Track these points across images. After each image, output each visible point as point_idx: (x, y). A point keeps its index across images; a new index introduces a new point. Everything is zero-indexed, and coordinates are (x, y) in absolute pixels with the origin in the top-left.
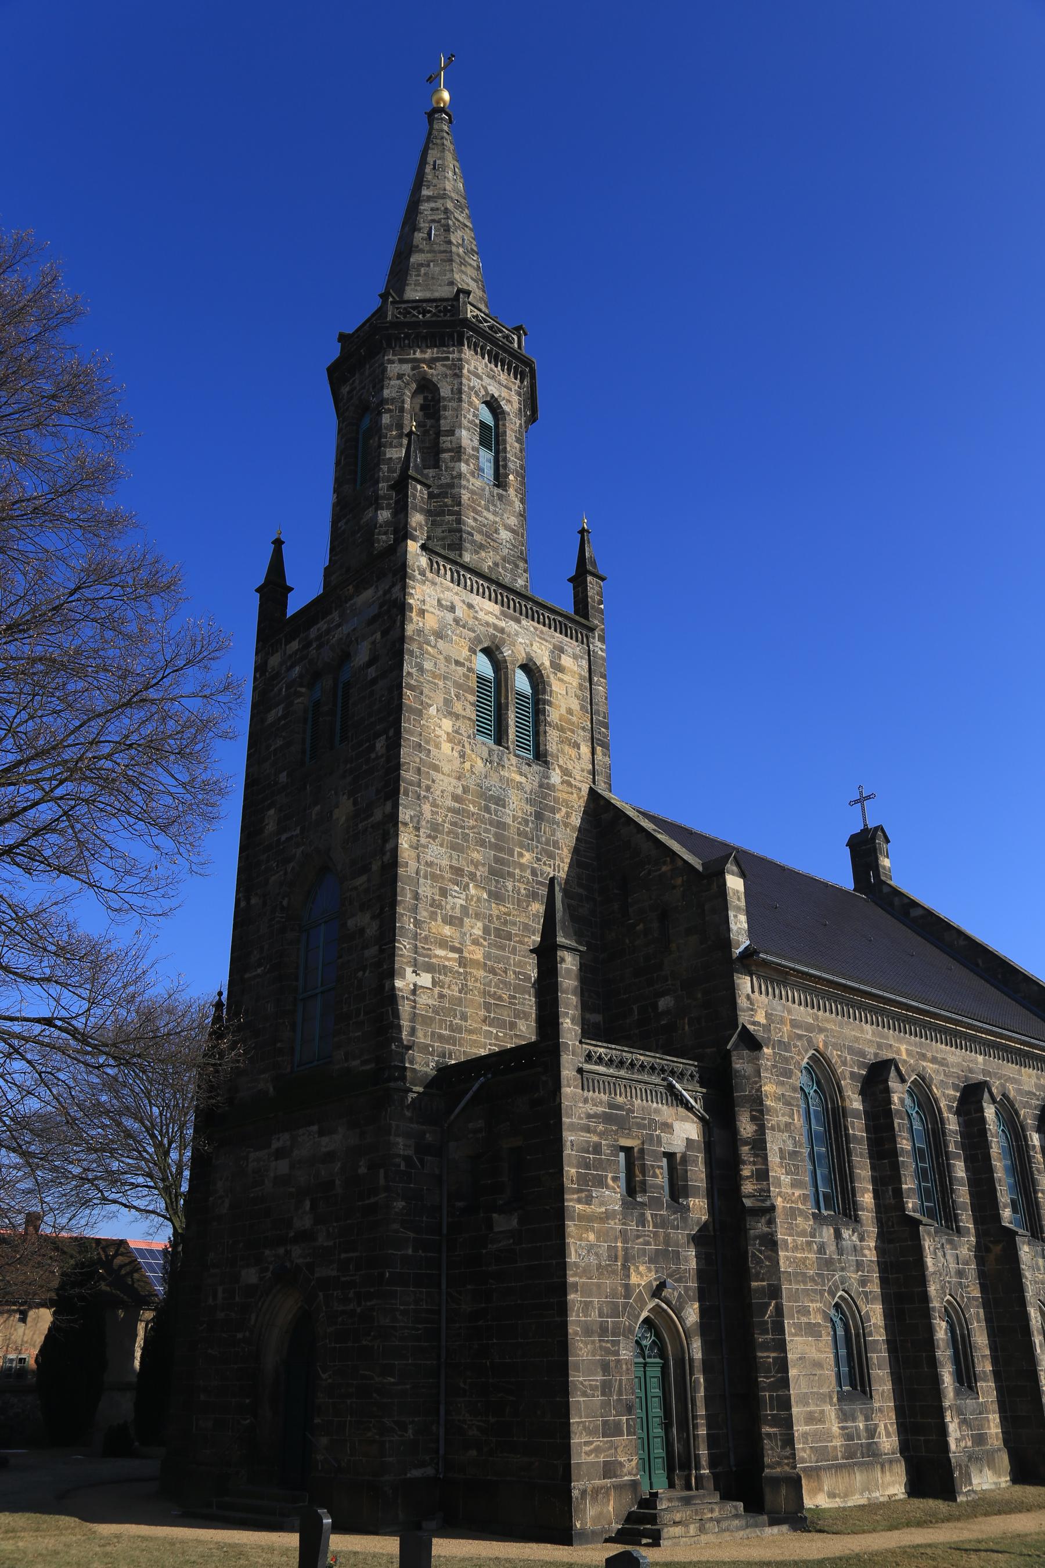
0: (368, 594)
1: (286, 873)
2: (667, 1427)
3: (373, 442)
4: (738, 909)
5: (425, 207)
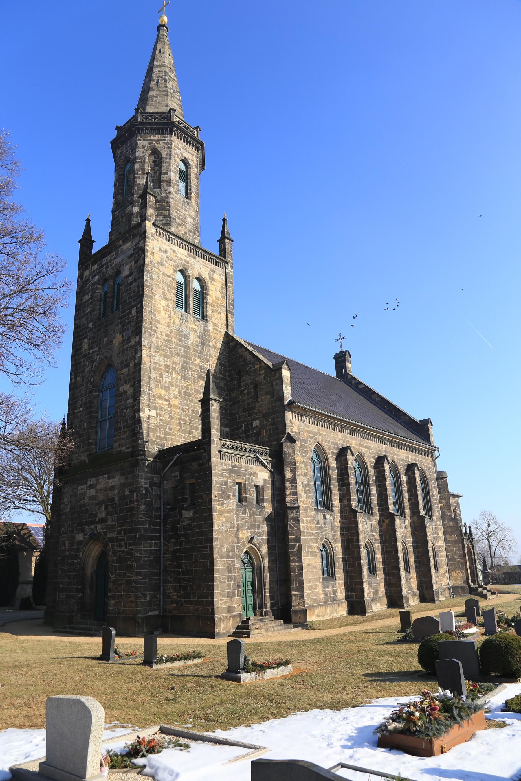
0: (128, 245)
1: (92, 367)
2: (254, 593)
3: (131, 177)
5: (155, 70)
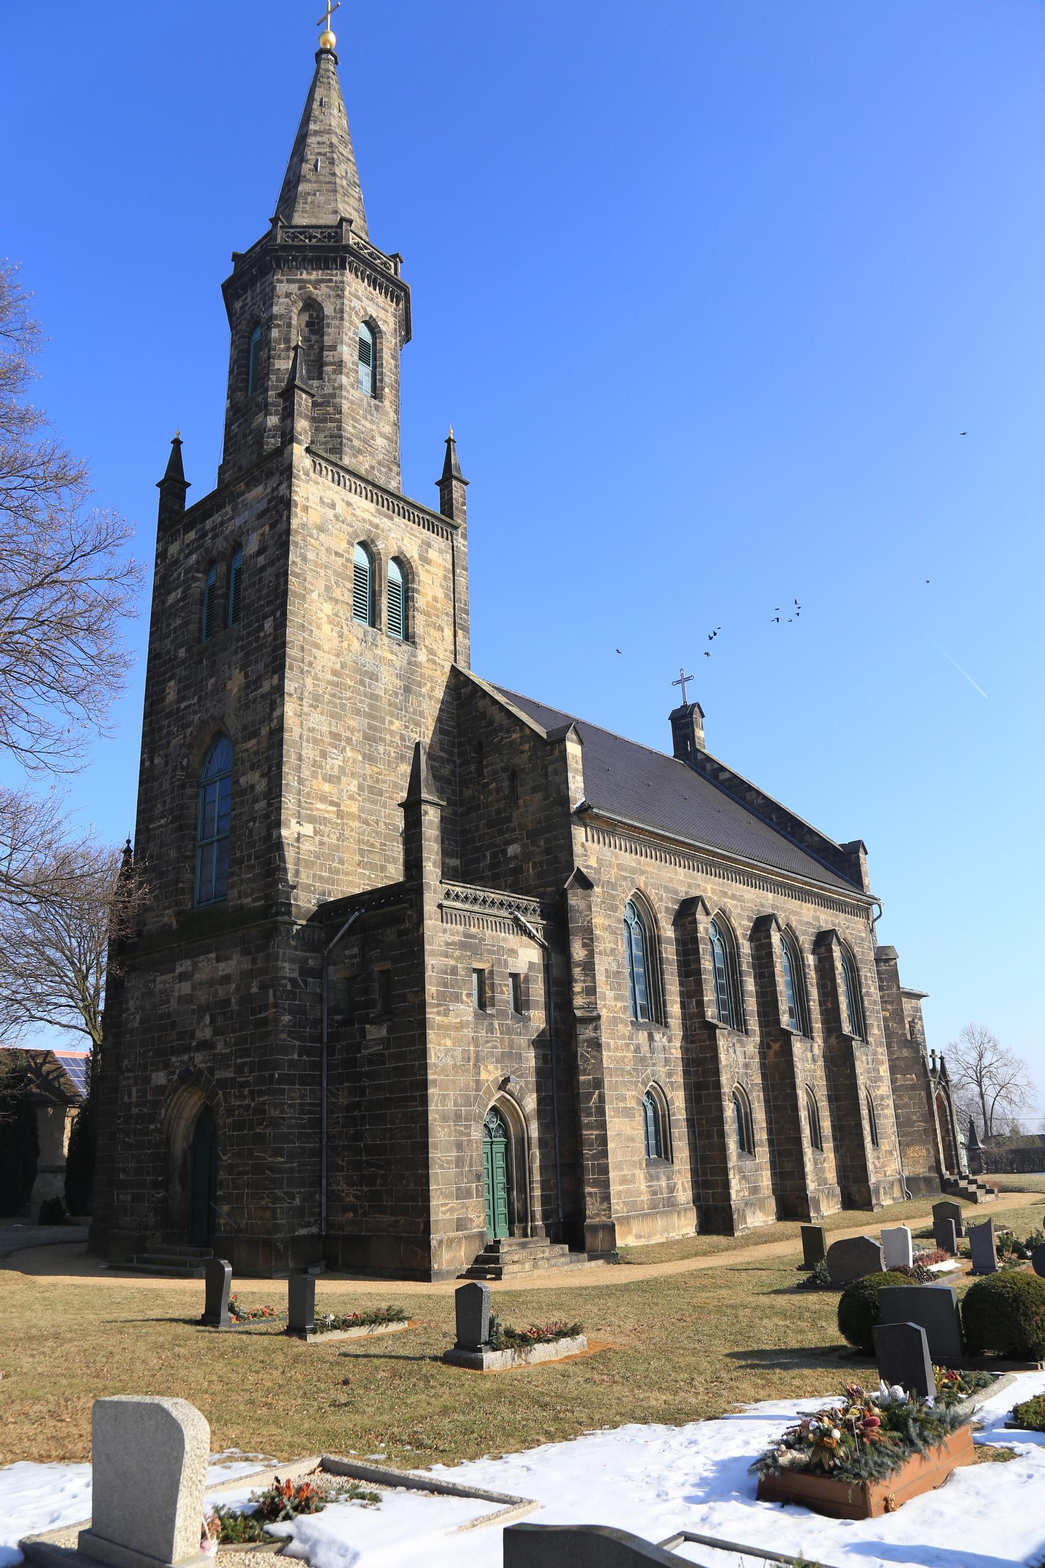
0: (258, 491)
1: (185, 737)
2: (509, 1191)
3: (263, 354)
4: (577, 770)
5: (312, 140)
